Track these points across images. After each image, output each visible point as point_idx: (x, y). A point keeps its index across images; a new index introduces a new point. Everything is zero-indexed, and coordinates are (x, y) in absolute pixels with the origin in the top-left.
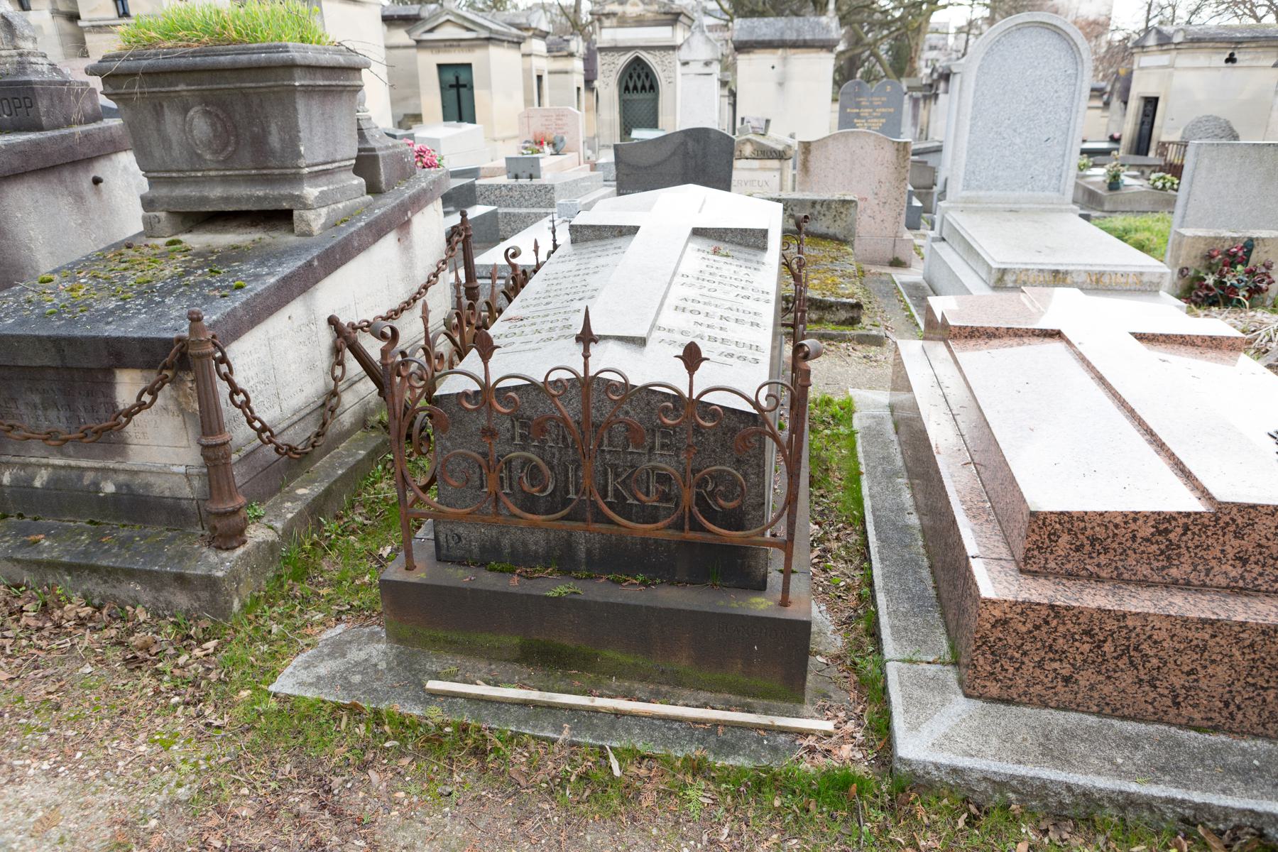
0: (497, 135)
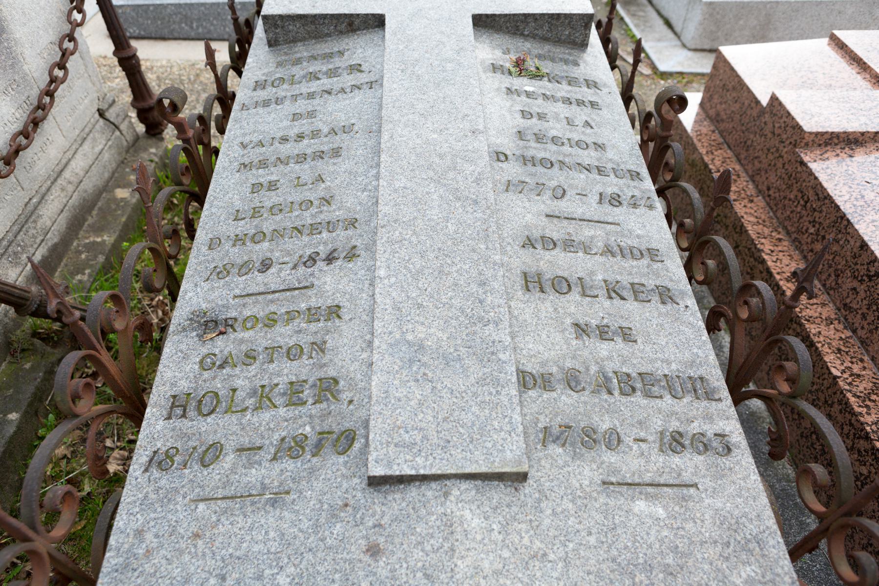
0: (107, 115)
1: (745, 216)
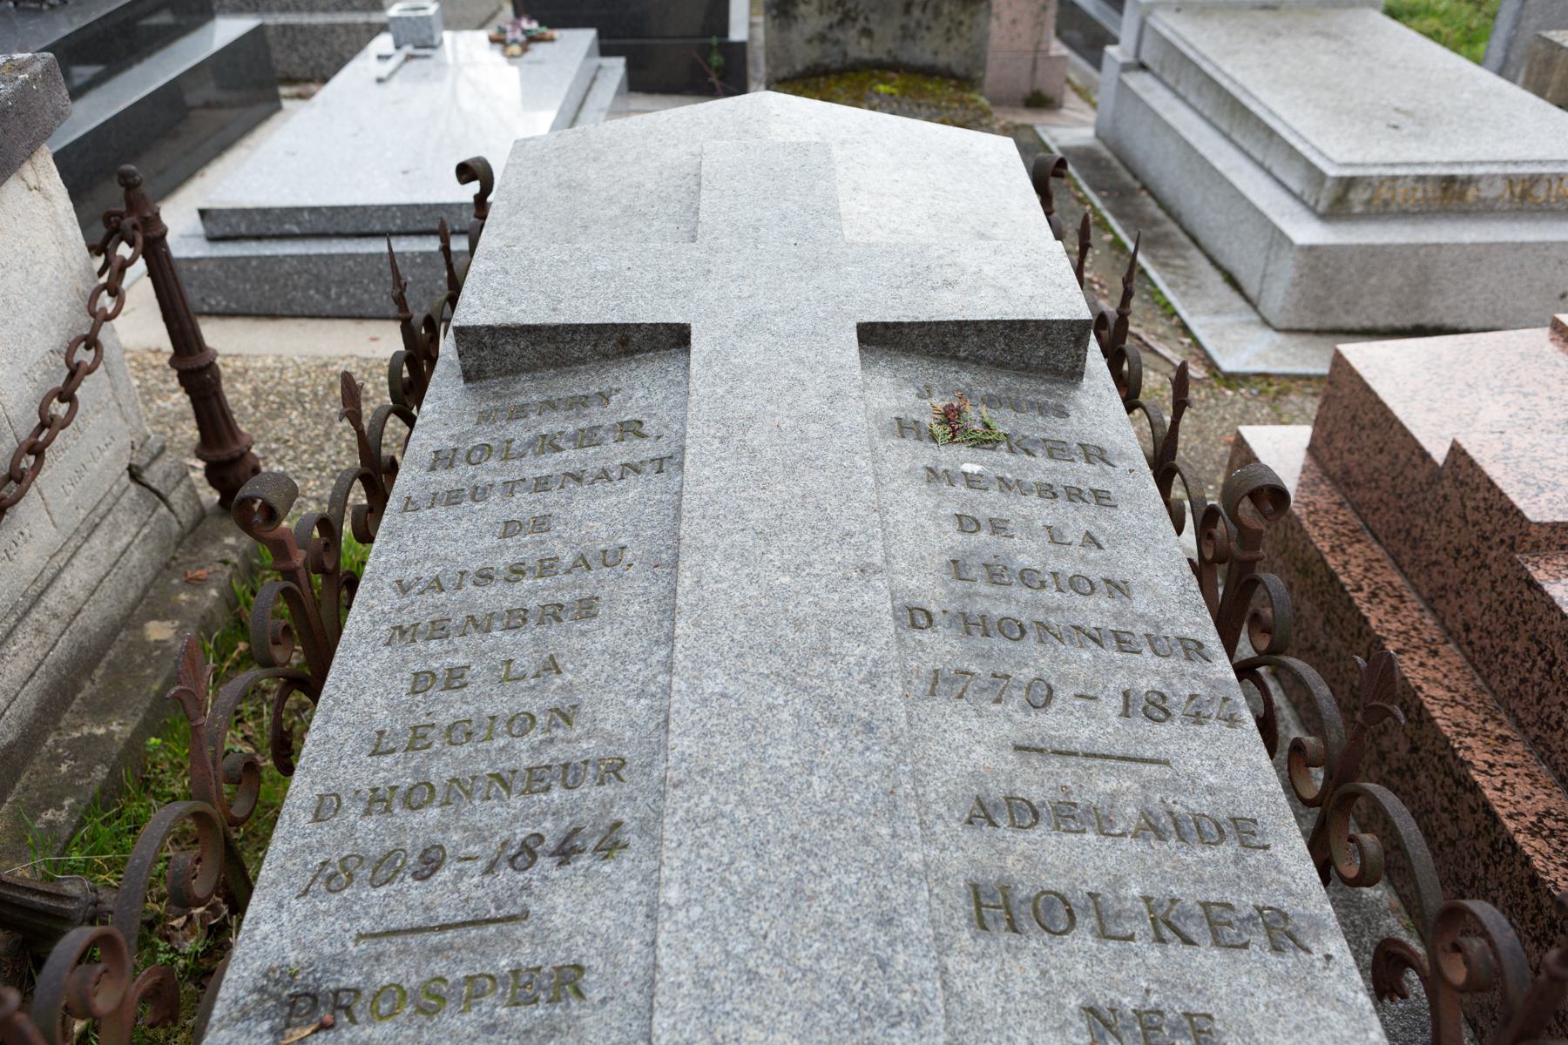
0: (146, 476)
1: (1425, 687)
